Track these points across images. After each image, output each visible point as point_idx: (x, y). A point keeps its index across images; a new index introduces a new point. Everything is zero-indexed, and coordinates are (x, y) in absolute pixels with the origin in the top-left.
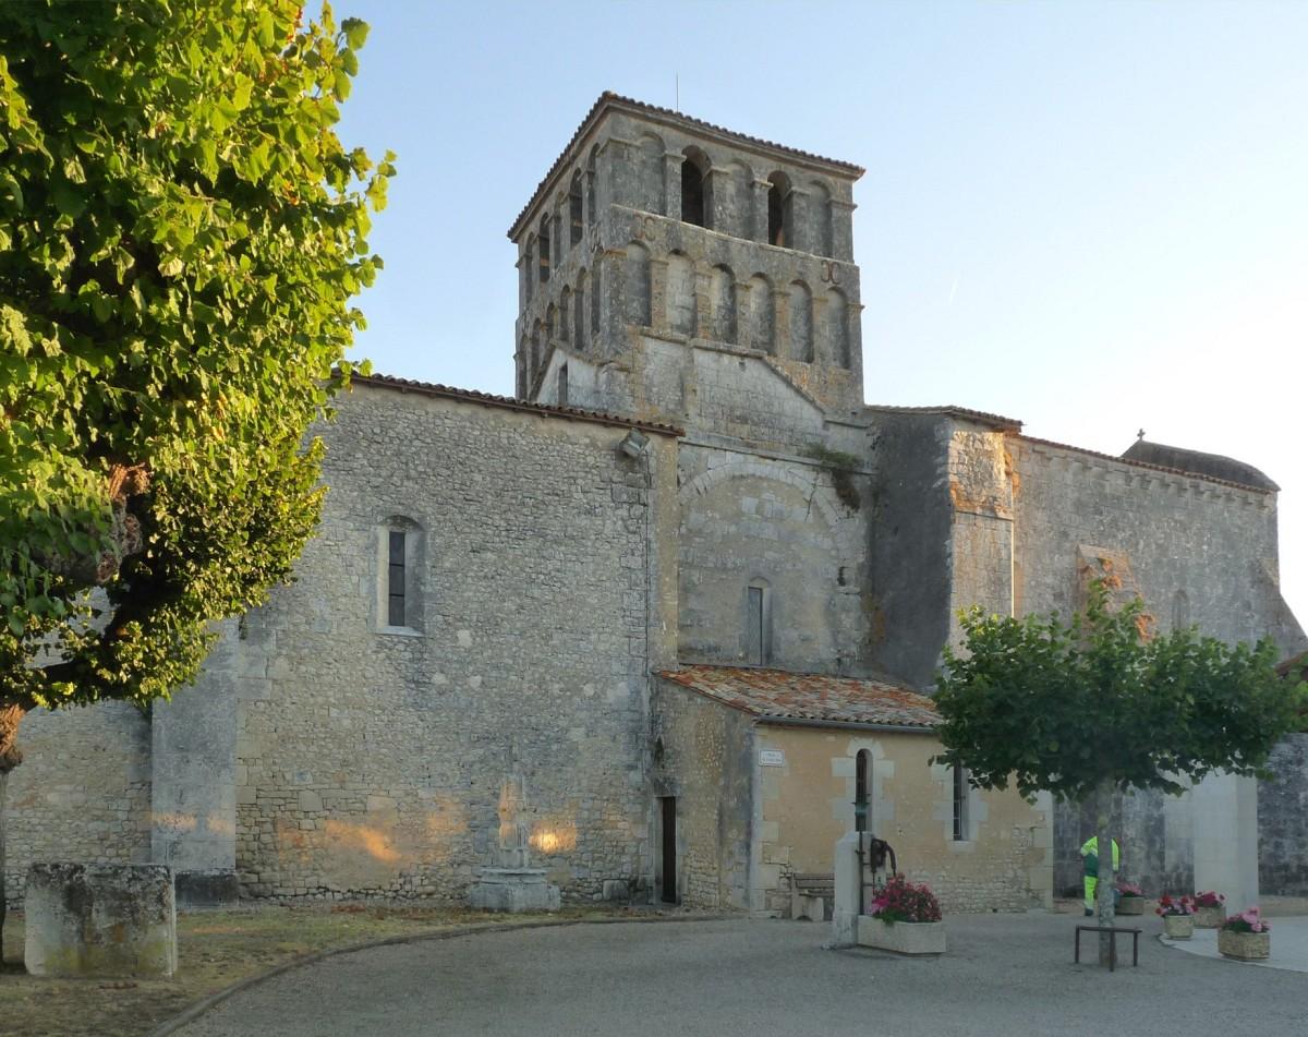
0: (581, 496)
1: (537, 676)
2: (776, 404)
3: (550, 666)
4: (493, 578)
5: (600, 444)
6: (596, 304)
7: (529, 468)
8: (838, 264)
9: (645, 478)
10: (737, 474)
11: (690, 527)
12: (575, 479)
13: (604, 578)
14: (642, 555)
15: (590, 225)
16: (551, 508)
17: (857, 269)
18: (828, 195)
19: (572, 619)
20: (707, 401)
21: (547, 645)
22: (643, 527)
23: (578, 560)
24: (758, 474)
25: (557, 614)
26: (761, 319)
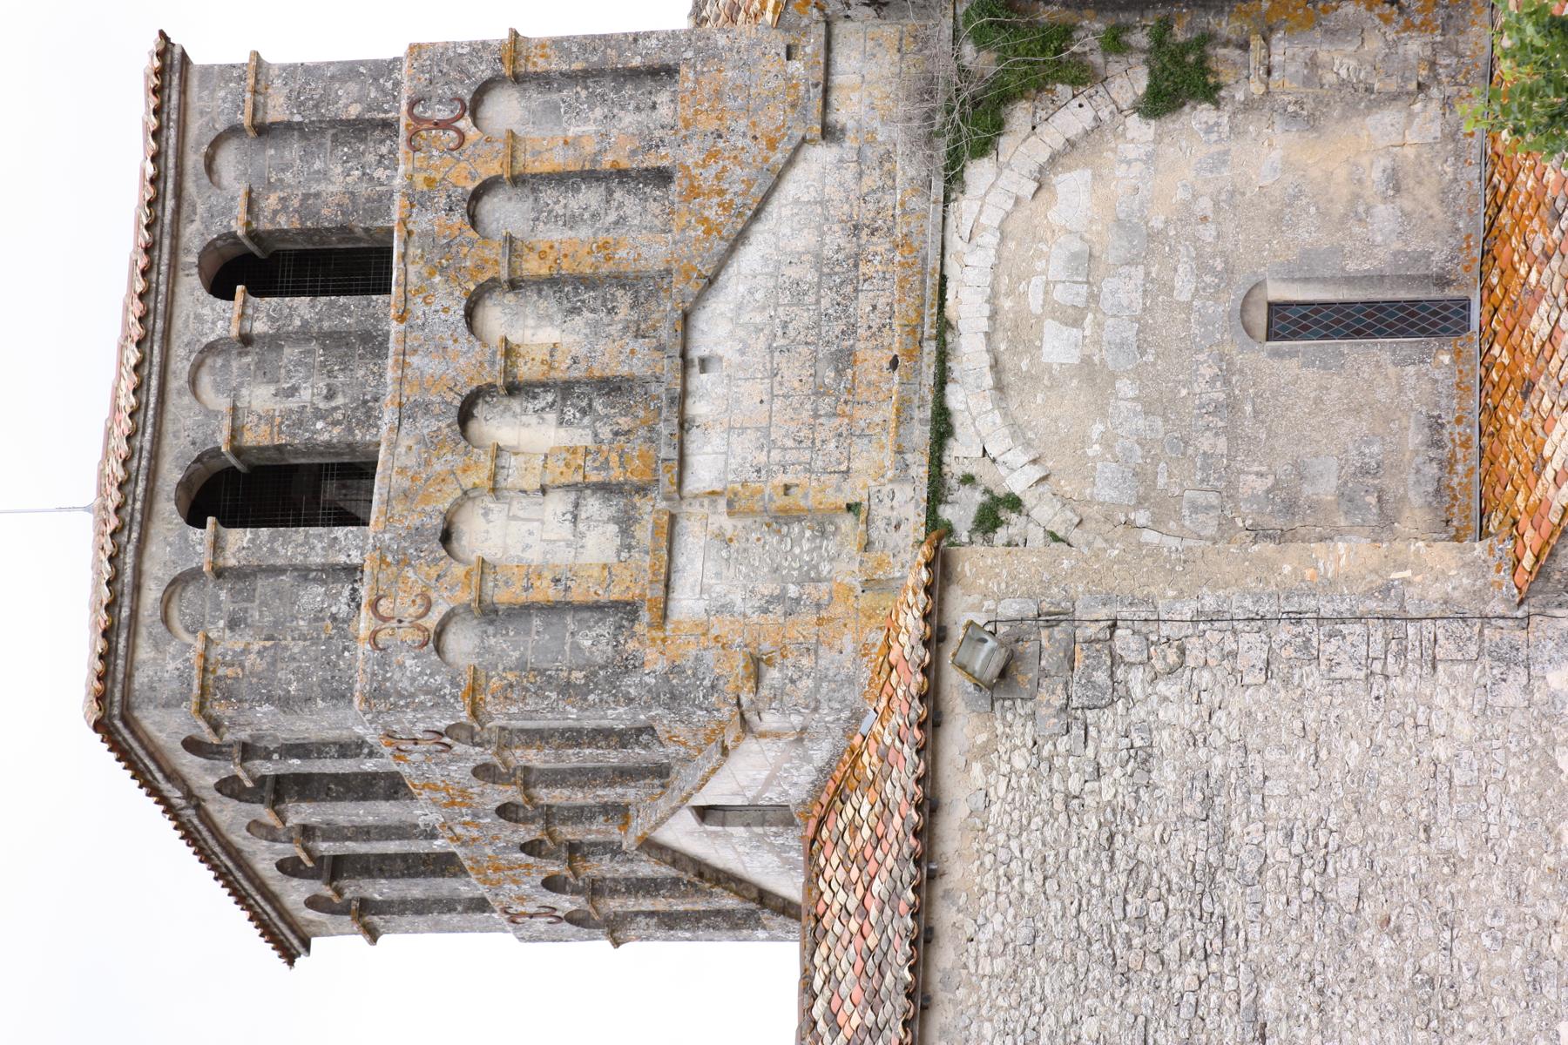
0: (1105, 781)
1: (1546, 887)
2: (793, 273)
3: (1520, 856)
4: (1321, 992)
5: (982, 738)
6: (574, 737)
7: (1056, 905)
8: (412, 104)
9: (1050, 625)
10: (988, 381)
11: (1128, 499)
12: (1069, 797)
13: (1297, 725)
14: (1235, 632)
15: (371, 754)
16: (1143, 853)
17: (416, 50)
18: (234, 131)
19: (1403, 800)
20: (807, 455)
21: (1471, 862)
22: (1165, 630)
23: (1259, 789)
24: (984, 324)
25: (1392, 838)
26: (574, 311)
